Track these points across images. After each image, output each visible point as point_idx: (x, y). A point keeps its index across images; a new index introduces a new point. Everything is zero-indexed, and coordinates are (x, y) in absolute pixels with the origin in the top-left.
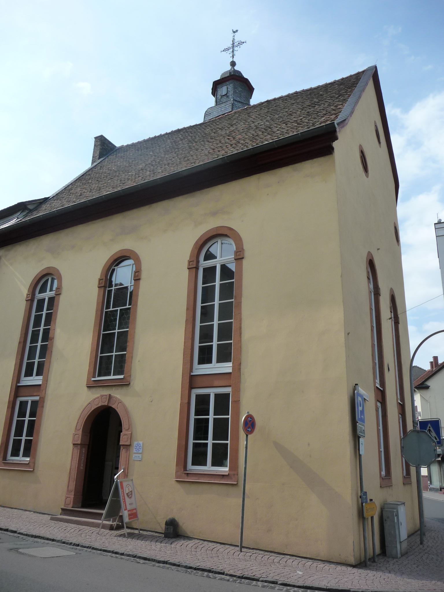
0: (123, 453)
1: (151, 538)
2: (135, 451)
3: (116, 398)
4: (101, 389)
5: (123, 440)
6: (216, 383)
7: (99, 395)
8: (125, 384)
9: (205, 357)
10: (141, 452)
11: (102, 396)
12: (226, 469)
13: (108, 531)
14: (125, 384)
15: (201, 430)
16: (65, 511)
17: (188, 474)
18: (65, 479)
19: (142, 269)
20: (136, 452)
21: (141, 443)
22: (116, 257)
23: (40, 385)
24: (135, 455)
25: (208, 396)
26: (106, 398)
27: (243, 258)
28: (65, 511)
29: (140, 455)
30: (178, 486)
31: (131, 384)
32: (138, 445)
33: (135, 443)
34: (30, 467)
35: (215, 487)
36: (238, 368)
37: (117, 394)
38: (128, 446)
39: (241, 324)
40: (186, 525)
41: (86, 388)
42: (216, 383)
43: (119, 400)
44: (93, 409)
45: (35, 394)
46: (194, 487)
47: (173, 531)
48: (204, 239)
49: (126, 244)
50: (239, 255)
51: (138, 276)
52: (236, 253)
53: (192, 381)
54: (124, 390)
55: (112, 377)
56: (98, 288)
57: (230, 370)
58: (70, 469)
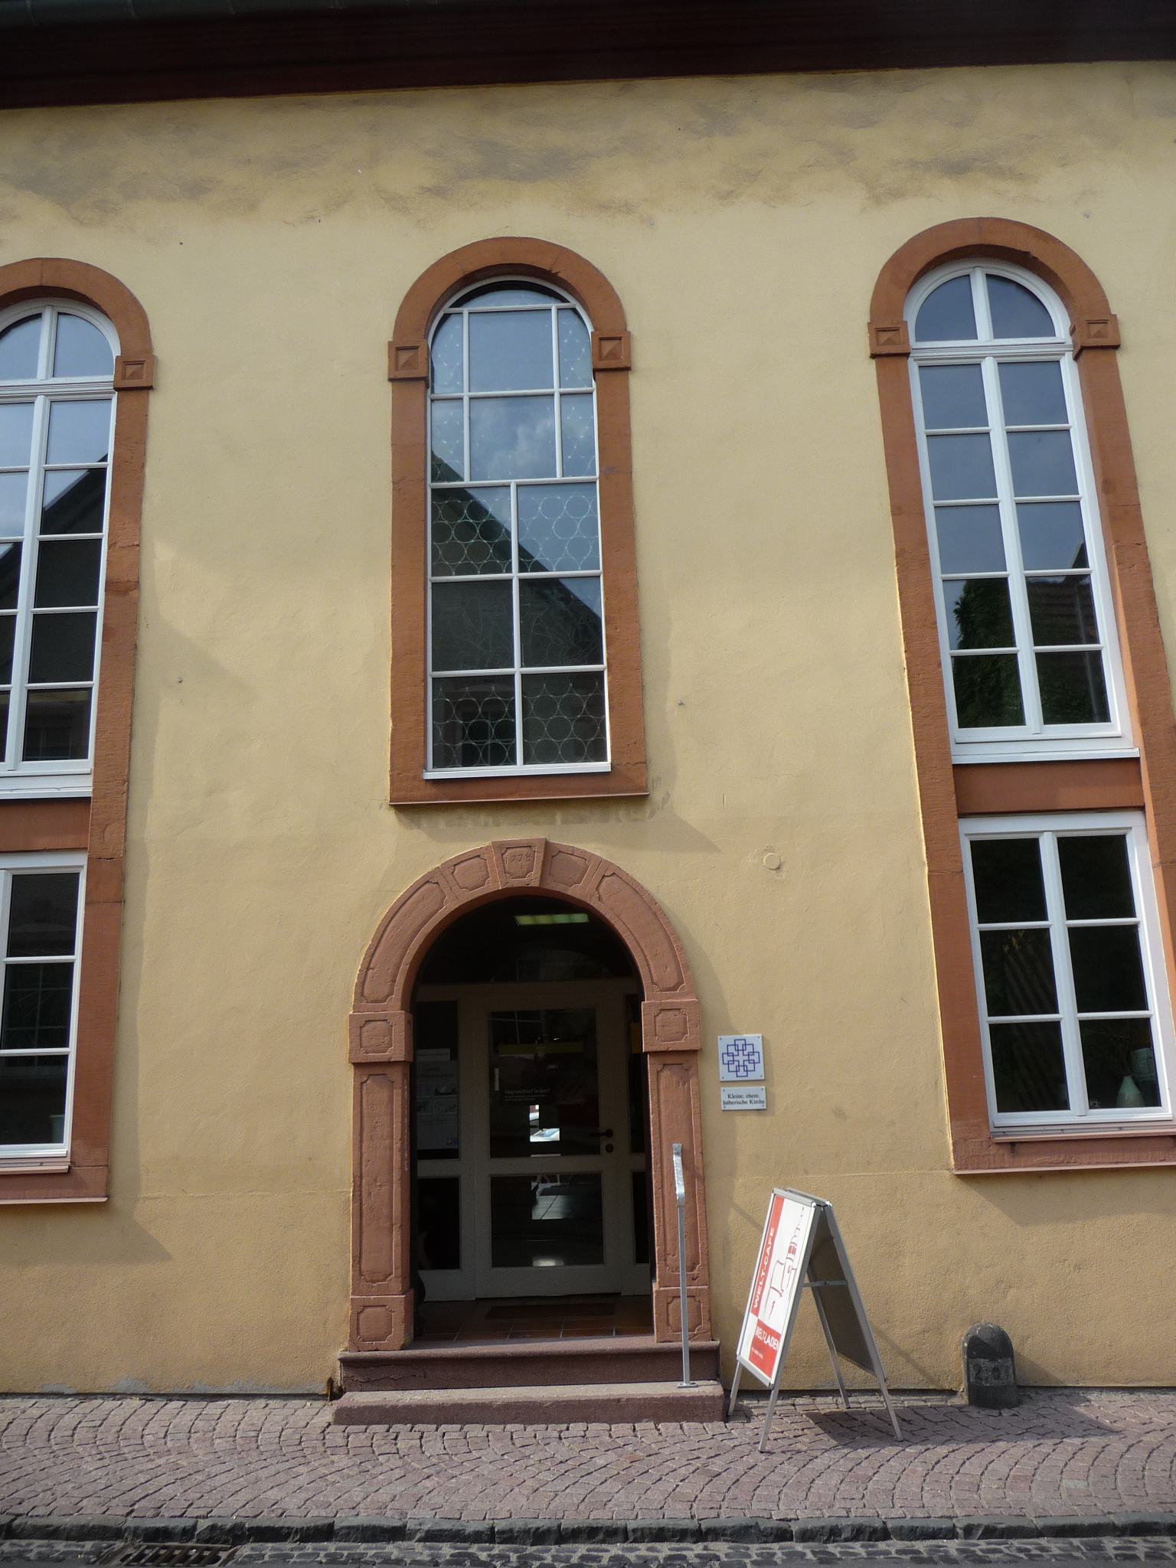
0: (663, 1091)
1: (915, 1429)
2: (724, 1073)
3: (585, 856)
4: (483, 817)
5: (656, 1032)
6: (1067, 798)
7: (488, 843)
8: (625, 794)
9: (986, 696)
10: (759, 1073)
11: (503, 848)
12: (61, 1149)
13: (716, 1427)
14: (625, 794)
15: (1016, 971)
16: (364, 1370)
17: (1013, 1144)
18: (338, 1227)
19: (632, 327)
20: (732, 1077)
21: (754, 1038)
22: (471, 267)
23: (84, 801)
24: (726, 1090)
25: (1029, 847)
26: (530, 857)
27: (150, 388)
28: (364, 1370)
29: (760, 1091)
30: (973, 1198)
31: (657, 795)
32: (742, 1047)
33: (724, 1042)
34: (79, 1187)
35: (1146, 1186)
36: (117, 776)
37: (589, 839)
38: (686, 1059)
39: (1150, 581)
40: (1040, 1346)
41: (390, 817)
42: (1069, 796)
43: (600, 861)
44: (450, 906)
45: (43, 842)
46: (1047, 1193)
47: (1000, 1383)
48: (998, 240)
49: (528, 217)
50: (134, 375)
51: (613, 355)
52: (124, 362)
53: (964, 789)
54: (619, 822)
55: (519, 768)
56: (389, 386)
57: (83, 787)
58: (358, 1178)
